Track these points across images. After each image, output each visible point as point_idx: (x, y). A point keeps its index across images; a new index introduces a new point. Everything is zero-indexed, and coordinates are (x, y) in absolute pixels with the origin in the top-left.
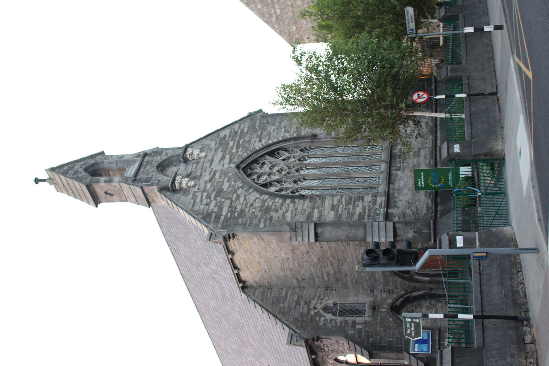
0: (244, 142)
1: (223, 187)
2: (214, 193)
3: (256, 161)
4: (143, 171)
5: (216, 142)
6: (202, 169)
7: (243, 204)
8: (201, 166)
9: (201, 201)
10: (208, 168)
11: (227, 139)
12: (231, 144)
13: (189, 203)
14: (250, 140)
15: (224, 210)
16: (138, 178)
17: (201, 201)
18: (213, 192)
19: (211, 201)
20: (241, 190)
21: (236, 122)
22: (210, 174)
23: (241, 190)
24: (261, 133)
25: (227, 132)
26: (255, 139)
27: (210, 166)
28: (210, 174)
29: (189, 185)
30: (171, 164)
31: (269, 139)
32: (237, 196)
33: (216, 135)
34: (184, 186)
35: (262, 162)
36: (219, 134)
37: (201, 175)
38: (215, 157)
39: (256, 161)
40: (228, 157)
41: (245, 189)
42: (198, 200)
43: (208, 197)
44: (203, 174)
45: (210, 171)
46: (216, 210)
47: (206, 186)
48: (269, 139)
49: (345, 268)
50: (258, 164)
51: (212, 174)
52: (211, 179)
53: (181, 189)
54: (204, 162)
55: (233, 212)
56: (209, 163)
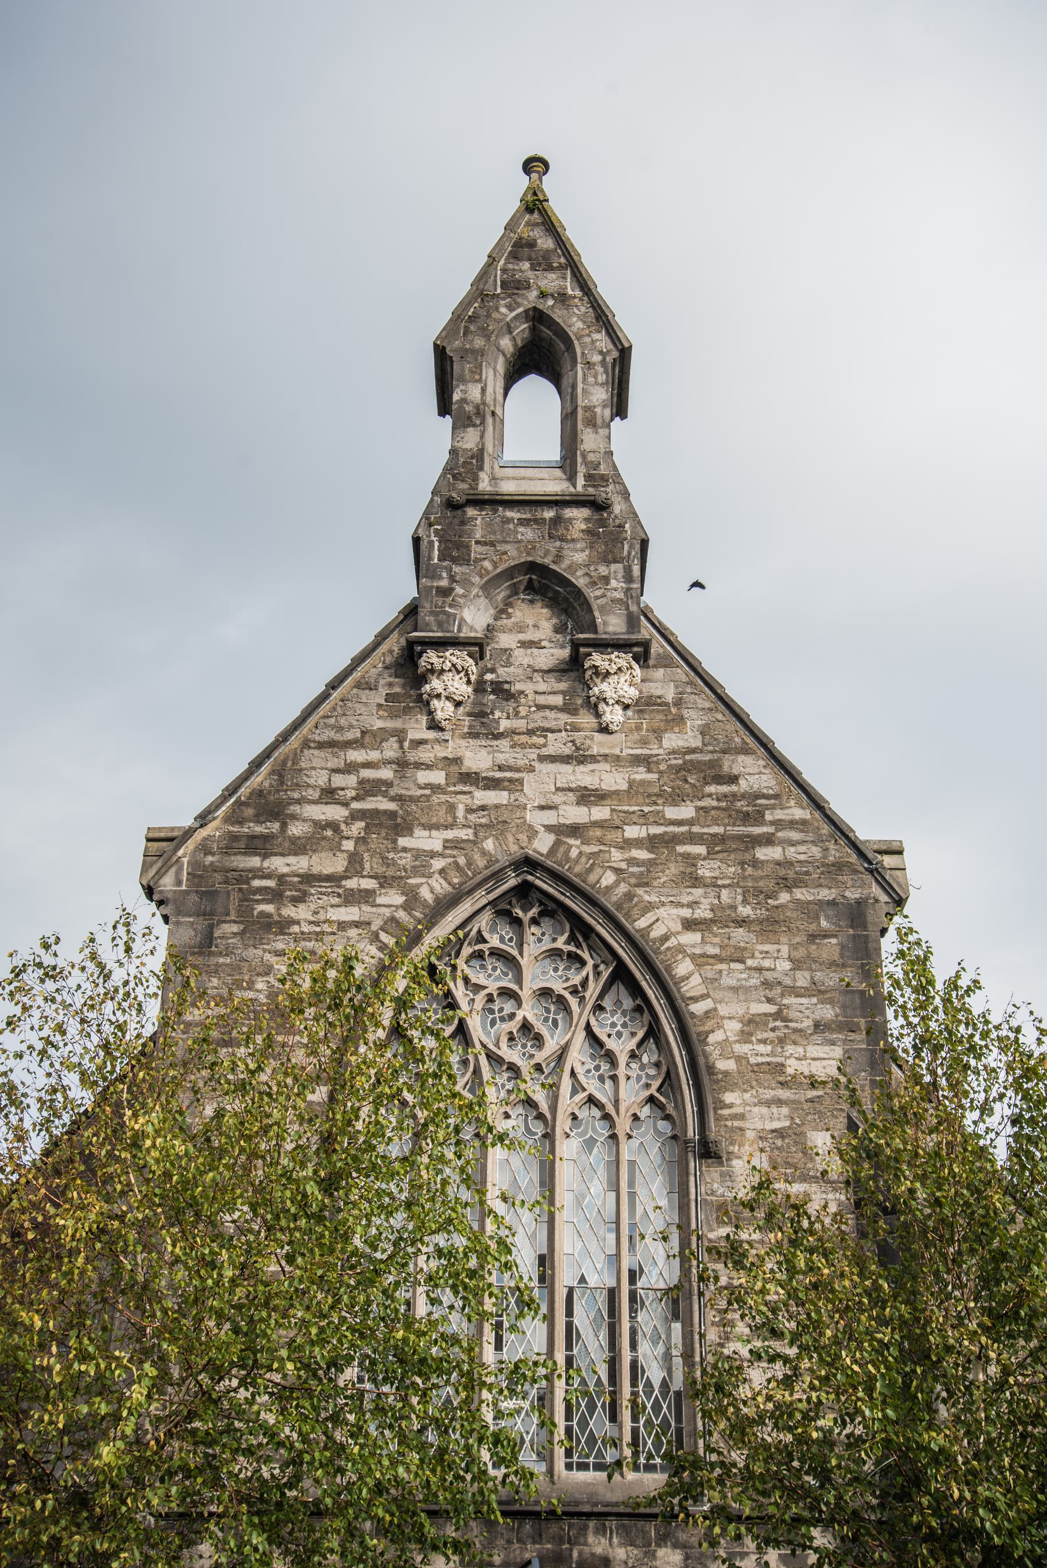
0: (690, 860)
1: (418, 832)
2: (392, 806)
3: (581, 931)
4: (510, 520)
5: (693, 751)
6: (530, 732)
7: (317, 923)
8: (552, 724)
9: (350, 768)
10: (533, 754)
11: (712, 789)
12: (686, 811)
13: (340, 729)
14: (696, 881)
15: (291, 859)
16: (471, 512)
17: (350, 768)
18: (399, 799)
19: (346, 805)
20: (399, 900)
21: (817, 803)
22: (501, 768)
23: (399, 900)
24: (742, 922)
25: (754, 775)
26: (705, 904)
27: (542, 759)
28: (501, 768)
29: (436, 703)
30: (565, 611)
31: (701, 960)
32: (366, 891)
33: (742, 736)
34: (604, 688)
35: (586, 955)
36: (745, 751)
37: (497, 736)
38: (604, 766)
39: (581, 931)
40: (600, 813)
41: (401, 915)
42: (356, 756)
43: (369, 789)
44: (504, 744)
45: (521, 763)
46: (296, 829)
47: (429, 767)
48: (701, 960)
49: (780, 1376)
50: (572, 939)
51: (498, 775)
52: (470, 778)
53: (421, 679)
54: (575, 728)
55: (276, 896)
56: (567, 750)
